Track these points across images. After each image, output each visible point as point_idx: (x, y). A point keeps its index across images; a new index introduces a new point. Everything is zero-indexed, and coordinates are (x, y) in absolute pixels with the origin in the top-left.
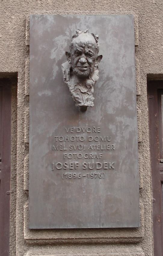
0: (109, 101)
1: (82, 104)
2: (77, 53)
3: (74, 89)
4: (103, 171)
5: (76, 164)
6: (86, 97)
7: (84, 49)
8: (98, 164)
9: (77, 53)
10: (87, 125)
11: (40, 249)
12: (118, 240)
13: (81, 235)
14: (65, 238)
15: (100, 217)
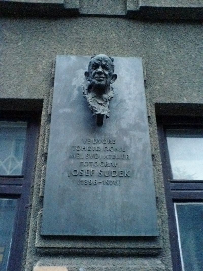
0: (123, 118)
1: (99, 112)
2: (95, 66)
3: (91, 100)
4: (119, 178)
5: (92, 171)
6: (102, 107)
7: (101, 62)
8: (114, 171)
9: (95, 66)
10: (103, 137)
11: (52, 260)
12: (135, 251)
13: (96, 244)
14: (78, 247)
15: (116, 224)
